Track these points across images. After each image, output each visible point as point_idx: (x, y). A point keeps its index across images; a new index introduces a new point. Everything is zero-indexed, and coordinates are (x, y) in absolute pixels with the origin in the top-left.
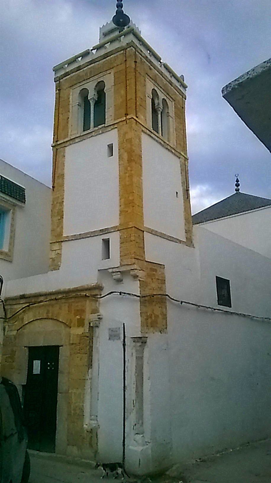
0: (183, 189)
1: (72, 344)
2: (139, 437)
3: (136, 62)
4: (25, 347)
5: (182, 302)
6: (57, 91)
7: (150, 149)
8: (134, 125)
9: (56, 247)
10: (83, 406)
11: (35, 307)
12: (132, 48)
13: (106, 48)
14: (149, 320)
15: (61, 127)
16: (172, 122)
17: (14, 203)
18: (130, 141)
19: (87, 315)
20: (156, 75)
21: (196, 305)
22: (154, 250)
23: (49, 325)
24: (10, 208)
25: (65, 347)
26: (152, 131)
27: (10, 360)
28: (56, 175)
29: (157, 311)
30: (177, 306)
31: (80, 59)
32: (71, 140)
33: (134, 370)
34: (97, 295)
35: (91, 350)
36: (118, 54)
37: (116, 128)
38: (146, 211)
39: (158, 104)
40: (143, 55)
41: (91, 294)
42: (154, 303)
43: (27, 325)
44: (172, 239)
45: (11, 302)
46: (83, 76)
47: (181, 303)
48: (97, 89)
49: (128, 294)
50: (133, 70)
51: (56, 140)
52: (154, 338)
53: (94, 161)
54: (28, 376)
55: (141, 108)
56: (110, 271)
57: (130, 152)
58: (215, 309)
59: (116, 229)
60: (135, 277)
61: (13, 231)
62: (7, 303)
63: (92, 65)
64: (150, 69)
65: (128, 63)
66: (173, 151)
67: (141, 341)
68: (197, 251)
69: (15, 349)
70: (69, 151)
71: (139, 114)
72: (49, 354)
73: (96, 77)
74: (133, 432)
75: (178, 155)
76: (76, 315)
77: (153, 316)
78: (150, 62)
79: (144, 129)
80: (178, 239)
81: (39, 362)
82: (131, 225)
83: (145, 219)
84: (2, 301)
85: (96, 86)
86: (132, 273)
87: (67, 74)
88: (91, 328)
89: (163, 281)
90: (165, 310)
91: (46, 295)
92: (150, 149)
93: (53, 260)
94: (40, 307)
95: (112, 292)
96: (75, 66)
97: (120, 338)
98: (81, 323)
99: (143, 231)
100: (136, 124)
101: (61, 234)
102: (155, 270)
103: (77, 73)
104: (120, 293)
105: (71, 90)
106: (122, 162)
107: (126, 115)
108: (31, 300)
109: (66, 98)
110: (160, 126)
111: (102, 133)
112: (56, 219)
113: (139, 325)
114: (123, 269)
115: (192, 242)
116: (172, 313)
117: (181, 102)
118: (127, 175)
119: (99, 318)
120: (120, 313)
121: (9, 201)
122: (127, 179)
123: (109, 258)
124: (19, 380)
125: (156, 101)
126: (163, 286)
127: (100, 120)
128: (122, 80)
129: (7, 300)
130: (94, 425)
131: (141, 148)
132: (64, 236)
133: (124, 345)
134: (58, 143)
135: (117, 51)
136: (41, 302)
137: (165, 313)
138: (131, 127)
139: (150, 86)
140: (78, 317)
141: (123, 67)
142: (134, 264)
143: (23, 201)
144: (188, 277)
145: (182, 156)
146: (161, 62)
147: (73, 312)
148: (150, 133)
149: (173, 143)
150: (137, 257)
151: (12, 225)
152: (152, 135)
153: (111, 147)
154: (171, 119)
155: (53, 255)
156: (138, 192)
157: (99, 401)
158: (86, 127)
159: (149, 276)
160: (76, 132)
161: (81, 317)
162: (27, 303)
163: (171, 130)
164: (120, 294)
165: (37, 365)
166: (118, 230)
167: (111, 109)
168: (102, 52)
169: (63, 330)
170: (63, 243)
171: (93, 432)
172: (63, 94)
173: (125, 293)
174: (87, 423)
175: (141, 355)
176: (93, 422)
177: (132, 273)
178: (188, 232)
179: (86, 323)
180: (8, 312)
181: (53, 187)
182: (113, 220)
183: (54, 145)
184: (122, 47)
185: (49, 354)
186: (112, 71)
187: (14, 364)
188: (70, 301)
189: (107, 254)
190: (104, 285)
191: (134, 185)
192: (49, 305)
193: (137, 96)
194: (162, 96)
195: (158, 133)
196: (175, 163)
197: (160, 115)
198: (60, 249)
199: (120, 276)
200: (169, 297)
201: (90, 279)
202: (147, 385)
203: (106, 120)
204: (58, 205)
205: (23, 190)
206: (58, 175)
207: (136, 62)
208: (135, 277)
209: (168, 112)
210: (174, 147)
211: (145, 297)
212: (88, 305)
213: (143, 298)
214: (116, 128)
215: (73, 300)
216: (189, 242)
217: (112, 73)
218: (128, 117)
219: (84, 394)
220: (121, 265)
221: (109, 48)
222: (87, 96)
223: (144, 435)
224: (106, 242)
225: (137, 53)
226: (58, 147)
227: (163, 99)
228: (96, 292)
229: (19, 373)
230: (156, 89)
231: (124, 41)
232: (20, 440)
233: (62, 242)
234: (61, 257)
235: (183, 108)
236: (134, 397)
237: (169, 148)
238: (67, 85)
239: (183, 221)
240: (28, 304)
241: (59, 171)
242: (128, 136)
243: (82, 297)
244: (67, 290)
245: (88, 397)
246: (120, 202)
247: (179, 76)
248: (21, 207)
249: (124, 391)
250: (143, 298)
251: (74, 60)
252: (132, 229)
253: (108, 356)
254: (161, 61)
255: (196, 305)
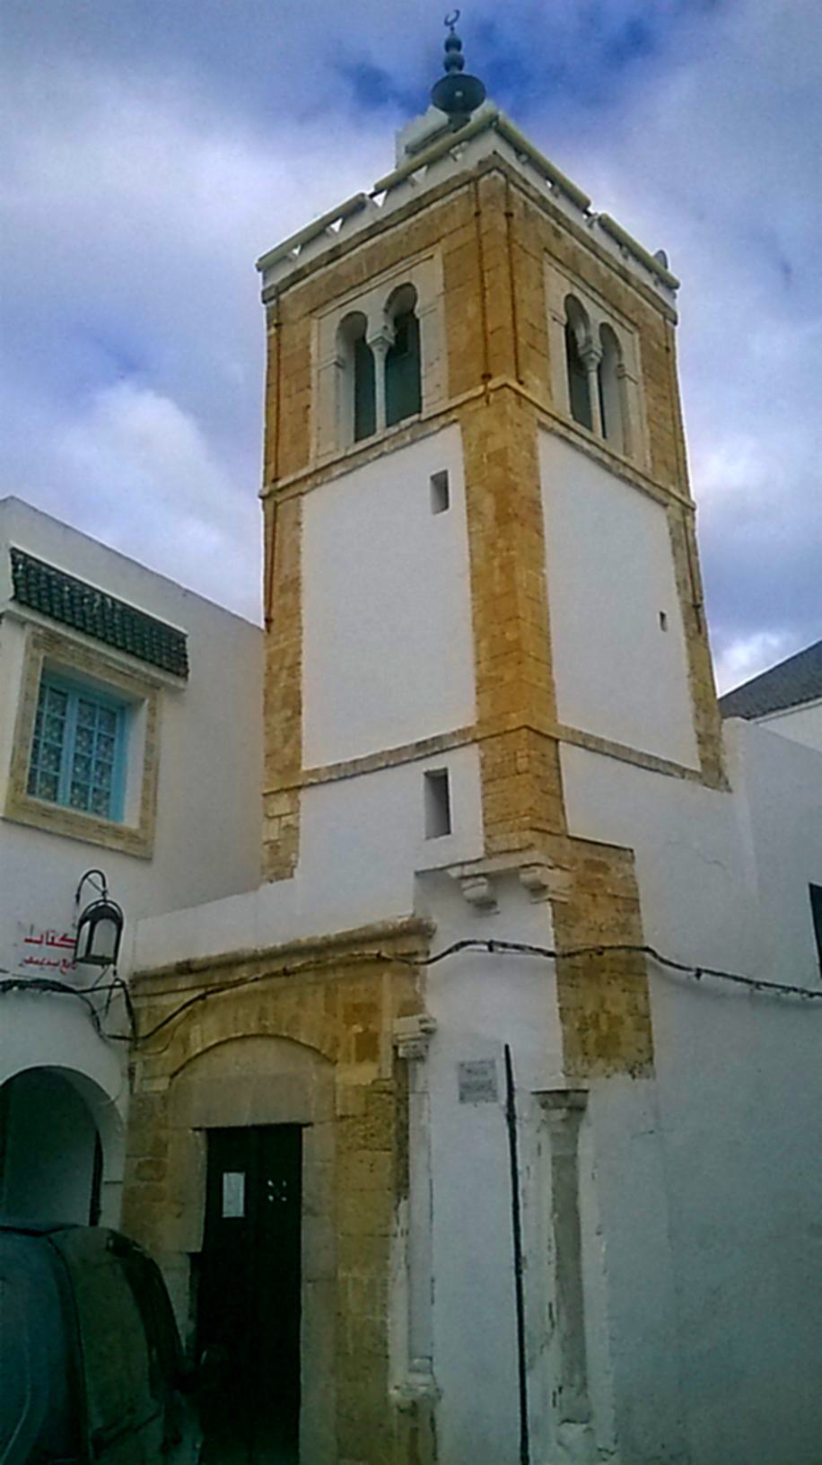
0: (684, 602)
1: (342, 1117)
2: (574, 1432)
3: (509, 215)
4: (195, 1129)
5: (699, 973)
6: (273, 330)
7: (567, 481)
8: (511, 407)
9: (282, 805)
10: (384, 1323)
11: (225, 1000)
12: (494, 173)
13: (413, 184)
14: (592, 1035)
15: (286, 438)
16: (636, 396)
17: (153, 679)
18: (500, 457)
19: (386, 1020)
20: (575, 253)
21: (749, 982)
22: (595, 801)
23: (268, 1059)
24: (140, 694)
25: (317, 1129)
26: (573, 424)
27: (148, 1172)
28: (277, 584)
29: (617, 999)
30: (686, 986)
31: (336, 226)
32: (317, 471)
33: (547, 1203)
34: (416, 954)
35: (402, 1135)
36: (452, 196)
37: (455, 421)
38: (560, 676)
39: (589, 340)
40: (532, 193)
41: (395, 951)
42: (606, 974)
43: (198, 1060)
44: (653, 765)
45: (148, 987)
46: (347, 277)
47: (698, 975)
48: (391, 311)
49: (516, 947)
50: (502, 242)
51: (272, 478)
52: (611, 1094)
53: (395, 527)
54: (206, 1223)
55: (533, 352)
56: (455, 873)
57: (503, 493)
58: (812, 995)
59: (464, 738)
60: (538, 889)
61: (151, 766)
62: (140, 990)
63: (373, 241)
64: (557, 234)
65: (484, 220)
66: (644, 484)
67: (568, 1104)
68: (740, 803)
69: (163, 1134)
70: (315, 507)
71: (527, 374)
72: (267, 1152)
73: (389, 274)
74: (554, 1415)
75: (660, 495)
76: (349, 1024)
77: (603, 1018)
78: (556, 214)
79: (544, 419)
80: (670, 764)
81: (225, 1176)
82: (515, 720)
83: (560, 703)
84: (123, 985)
85: (389, 302)
86: (526, 877)
87: (298, 276)
88: (401, 1065)
89: (632, 904)
90: (641, 997)
91: (255, 959)
92: (567, 481)
93: (274, 846)
94: (239, 997)
95: (463, 944)
96: (323, 247)
97: (495, 1097)
98: (367, 1048)
99: (557, 741)
100: (519, 404)
101: (295, 765)
102: (601, 864)
103: (331, 266)
104: (491, 945)
105: (315, 322)
106: (477, 526)
107: (487, 377)
108: (209, 978)
109: (300, 347)
110: (596, 407)
111: (413, 441)
112: (278, 718)
113: (558, 1050)
114: (494, 866)
115: (721, 774)
116: (668, 1011)
117: (660, 332)
118: (496, 563)
119: (423, 1031)
120: (493, 1010)
121: (136, 671)
122: (497, 576)
123: (449, 832)
124: (175, 1240)
125: (581, 334)
126: (634, 918)
127: (406, 401)
128: (469, 275)
129: (139, 979)
130: (423, 1389)
131: (538, 477)
132: (304, 768)
133: (511, 1118)
134: (280, 484)
135: (449, 187)
136: (242, 981)
137: (641, 1007)
138: (502, 415)
139: (558, 287)
140: (358, 1029)
141: (469, 234)
142: (531, 846)
143: (182, 670)
144: (713, 886)
145: (672, 501)
146: (589, 214)
147: (341, 1012)
148: (562, 430)
149: (641, 459)
150: (539, 825)
151: (150, 748)
152: (573, 437)
153: (440, 483)
154: (630, 384)
155: (273, 831)
156: (534, 614)
157: (436, 1308)
158: (363, 427)
159: (581, 884)
160: (331, 446)
161: (366, 1030)
162: (199, 987)
163: (634, 420)
164: (491, 949)
165: (234, 1184)
166: (475, 741)
167: (436, 365)
168: (404, 197)
169: (313, 1074)
170: (302, 795)
171: (419, 1413)
172: (291, 334)
173: (504, 945)
174: (401, 1383)
175: (569, 1152)
176: (421, 1379)
177: (526, 877)
178: (707, 740)
179: (385, 1048)
180: (143, 1019)
181: (268, 621)
182: (458, 709)
183: (266, 492)
184: (464, 174)
185: (267, 1152)
186: (438, 252)
187: (164, 1184)
188: (331, 976)
189: (442, 821)
190: (435, 920)
191: (520, 594)
192: (264, 993)
193: (519, 317)
194: (597, 316)
195: (590, 429)
196: (654, 522)
197: (593, 376)
198: (294, 812)
199: (489, 888)
200: (655, 954)
201: (392, 904)
202: (594, 1252)
203: (424, 402)
204: (284, 674)
205: (180, 639)
206: (281, 581)
207: (509, 215)
208: (538, 889)
209: (620, 366)
210: (648, 472)
211: (570, 955)
212: (388, 989)
213: (563, 956)
214: (455, 421)
215: (340, 974)
216: (713, 773)
217: (438, 257)
218: (491, 385)
219: (385, 1284)
220: (490, 854)
221: (425, 181)
222: (364, 339)
223: (592, 1424)
224: (438, 782)
225: (512, 188)
226: (280, 499)
227: (603, 326)
228: (413, 944)
229: (179, 1216)
230: (577, 294)
231: (468, 159)
232: (171, 1443)
233: (299, 788)
234: (297, 837)
235: (669, 350)
236: (551, 1294)
237: (629, 474)
238: (302, 308)
239: (687, 707)
240: (201, 992)
241: (284, 572)
242: (495, 444)
243: (366, 962)
244: (318, 942)
245: (398, 1296)
246: (477, 654)
247: (652, 253)
248: (176, 692)
249: (518, 1272)
250: (563, 956)
251: (319, 231)
252: (520, 732)
253: (458, 1149)
254: (591, 210)
255: (749, 982)
